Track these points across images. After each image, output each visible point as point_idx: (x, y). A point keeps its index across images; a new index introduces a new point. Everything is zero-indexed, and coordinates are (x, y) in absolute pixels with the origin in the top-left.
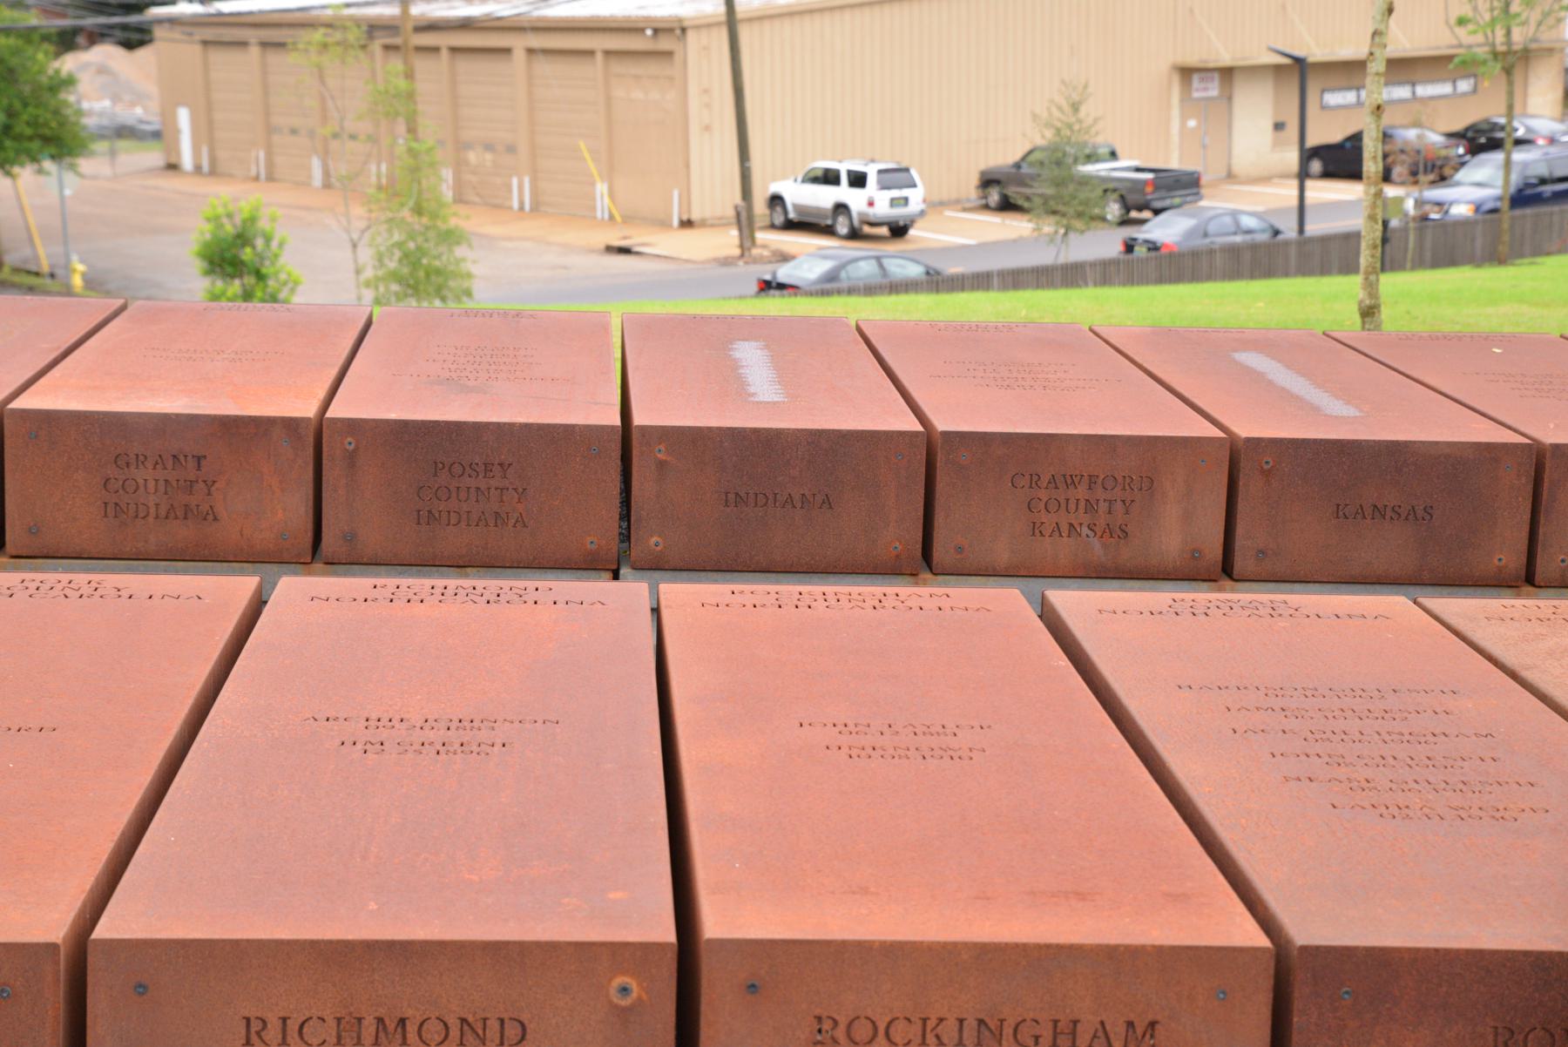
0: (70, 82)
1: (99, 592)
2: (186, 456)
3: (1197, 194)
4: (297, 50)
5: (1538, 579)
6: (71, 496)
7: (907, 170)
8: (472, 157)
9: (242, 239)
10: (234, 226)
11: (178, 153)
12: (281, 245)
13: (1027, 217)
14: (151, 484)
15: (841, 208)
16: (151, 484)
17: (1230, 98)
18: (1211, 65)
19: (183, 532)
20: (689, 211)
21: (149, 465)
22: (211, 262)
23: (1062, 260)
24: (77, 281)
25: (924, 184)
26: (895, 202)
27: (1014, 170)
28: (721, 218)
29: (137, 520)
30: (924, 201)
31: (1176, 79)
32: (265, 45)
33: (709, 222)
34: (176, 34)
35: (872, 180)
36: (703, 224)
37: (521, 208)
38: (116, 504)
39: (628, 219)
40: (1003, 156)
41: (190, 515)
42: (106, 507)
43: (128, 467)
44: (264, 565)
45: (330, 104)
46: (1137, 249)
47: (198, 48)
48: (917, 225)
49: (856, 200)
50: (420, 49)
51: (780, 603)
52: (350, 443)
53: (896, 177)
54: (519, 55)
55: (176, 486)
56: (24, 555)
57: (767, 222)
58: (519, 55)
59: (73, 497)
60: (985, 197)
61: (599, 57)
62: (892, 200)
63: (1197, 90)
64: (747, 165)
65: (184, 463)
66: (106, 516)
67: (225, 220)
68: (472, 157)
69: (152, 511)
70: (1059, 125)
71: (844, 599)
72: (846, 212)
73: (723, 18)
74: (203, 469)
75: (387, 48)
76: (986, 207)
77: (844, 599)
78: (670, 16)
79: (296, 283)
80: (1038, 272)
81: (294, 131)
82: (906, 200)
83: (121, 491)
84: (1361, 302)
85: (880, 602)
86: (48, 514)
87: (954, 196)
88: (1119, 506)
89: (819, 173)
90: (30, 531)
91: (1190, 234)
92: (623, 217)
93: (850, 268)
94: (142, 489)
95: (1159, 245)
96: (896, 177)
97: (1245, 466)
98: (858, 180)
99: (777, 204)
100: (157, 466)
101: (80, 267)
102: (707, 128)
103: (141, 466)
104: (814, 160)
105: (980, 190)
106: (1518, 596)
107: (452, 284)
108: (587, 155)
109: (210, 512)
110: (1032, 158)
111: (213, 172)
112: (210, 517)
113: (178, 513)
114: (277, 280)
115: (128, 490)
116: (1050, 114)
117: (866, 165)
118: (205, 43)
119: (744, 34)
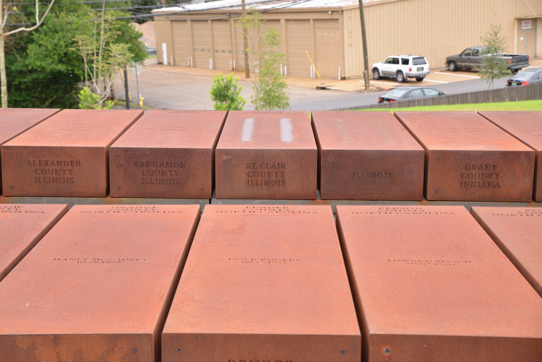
0: (141, 35)
2: (490, 165)
3: (528, 63)
4: (238, 22)
5: (428, 198)
6: (450, 179)
7: (423, 58)
9: (227, 88)
10: (224, 83)
11: (162, 59)
12: (240, 90)
13: (477, 74)
14: (477, 175)
15: (399, 72)
16: (477, 175)
17: (536, 29)
18: (530, 17)
19: (487, 192)
20: (344, 75)
21: (477, 169)
22: (216, 96)
23: (491, 89)
24: (141, 103)
26: (419, 69)
27: (459, 57)
28: (355, 76)
29: (472, 188)
30: (429, 69)
31: (516, 22)
32: (192, 21)
33: (351, 78)
34: (162, 18)
35: (411, 62)
36: (349, 78)
37: (313, 77)
38: (465, 182)
39: (323, 77)
40: (455, 52)
41: (490, 185)
42: (461, 183)
43: (470, 169)
44: (172, 199)
45: (249, 41)
46: (513, 83)
47: (169, 22)
48: (426, 77)
49: (405, 69)
51: (380, 212)
52: (225, 158)
53: (419, 60)
54: (283, 22)
55: (486, 176)
56: (433, 200)
57: (373, 77)
58: (283, 22)
59: (451, 180)
60: (449, 67)
61: (312, 21)
62: (418, 68)
63: (524, 27)
64: (367, 57)
65: (489, 168)
66: (461, 186)
67: (221, 81)
69: (477, 184)
70: (490, 40)
71: (263, 209)
72: (401, 73)
73: (358, 6)
74: (496, 170)
76: (449, 70)
77: (263, 209)
78: (337, 6)
79: (244, 103)
80: (484, 92)
81: (202, 50)
82: (423, 68)
83: (467, 178)
84: (212, 98)
85: (415, 211)
86: (442, 186)
87: (436, 67)
89: (391, 60)
91: (532, 78)
92: (321, 77)
93: (412, 93)
94: (474, 177)
95: (521, 82)
96: (419, 60)
98: (406, 62)
99: (375, 71)
100: (52, 165)
101: (142, 99)
102: (351, 45)
103: (474, 169)
104: (391, 55)
105: (447, 64)
106: (531, 206)
107: (282, 101)
108: (309, 56)
109: (497, 184)
110: (466, 52)
111: (174, 65)
112: (497, 186)
113: (486, 185)
114: (238, 102)
115: (469, 177)
116: (487, 37)
117: (408, 57)
118: (172, 21)
119: (365, 11)
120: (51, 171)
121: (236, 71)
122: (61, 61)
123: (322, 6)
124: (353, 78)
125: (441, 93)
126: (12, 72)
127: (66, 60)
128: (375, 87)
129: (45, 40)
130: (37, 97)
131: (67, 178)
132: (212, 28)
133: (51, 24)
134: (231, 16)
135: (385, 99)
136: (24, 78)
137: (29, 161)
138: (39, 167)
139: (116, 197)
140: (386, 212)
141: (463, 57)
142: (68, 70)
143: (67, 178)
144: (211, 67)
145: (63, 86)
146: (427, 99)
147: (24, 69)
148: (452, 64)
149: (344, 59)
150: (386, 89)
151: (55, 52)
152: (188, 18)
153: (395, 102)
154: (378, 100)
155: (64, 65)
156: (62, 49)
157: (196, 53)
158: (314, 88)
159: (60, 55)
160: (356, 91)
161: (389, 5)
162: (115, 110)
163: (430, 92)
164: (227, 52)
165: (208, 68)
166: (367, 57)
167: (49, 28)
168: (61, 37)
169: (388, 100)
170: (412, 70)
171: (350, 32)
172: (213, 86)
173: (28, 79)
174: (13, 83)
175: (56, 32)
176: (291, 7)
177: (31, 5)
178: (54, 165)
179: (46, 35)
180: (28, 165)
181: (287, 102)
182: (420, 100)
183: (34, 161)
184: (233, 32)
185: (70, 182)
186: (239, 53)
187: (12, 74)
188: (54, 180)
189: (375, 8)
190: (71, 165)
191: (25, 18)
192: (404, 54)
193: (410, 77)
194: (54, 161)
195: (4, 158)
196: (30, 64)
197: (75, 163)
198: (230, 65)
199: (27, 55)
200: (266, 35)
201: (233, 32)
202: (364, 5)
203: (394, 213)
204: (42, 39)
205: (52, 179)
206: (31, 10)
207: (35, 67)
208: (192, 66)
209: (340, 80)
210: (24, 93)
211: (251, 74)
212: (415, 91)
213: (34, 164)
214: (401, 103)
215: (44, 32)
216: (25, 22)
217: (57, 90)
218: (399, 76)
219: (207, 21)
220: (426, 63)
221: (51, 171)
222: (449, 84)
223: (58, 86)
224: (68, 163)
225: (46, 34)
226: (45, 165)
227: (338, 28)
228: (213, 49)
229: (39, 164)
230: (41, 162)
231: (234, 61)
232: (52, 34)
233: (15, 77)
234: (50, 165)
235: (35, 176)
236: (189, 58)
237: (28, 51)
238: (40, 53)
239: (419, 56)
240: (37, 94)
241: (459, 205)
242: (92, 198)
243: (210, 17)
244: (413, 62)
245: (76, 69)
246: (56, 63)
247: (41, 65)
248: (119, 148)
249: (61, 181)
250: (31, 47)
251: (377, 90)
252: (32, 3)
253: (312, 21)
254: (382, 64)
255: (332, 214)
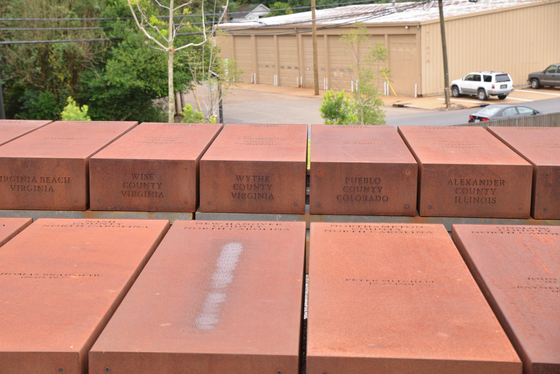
1: (112, 225)
7: (506, 75)
8: (335, 74)
9: (338, 104)
15: (481, 89)
20: (421, 92)
22: (326, 113)
25: (513, 80)
27: (543, 74)
28: (432, 94)
33: (428, 95)
35: (494, 79)
36: (426, 96)
37: (387, 94)
39: (399, 95)
40: (539, 68)
47: (232, 38)
48: (509, 95)
49: (487, 86)
50: (318, 36)
53: (503, 77)
60: (531, 84)
61: (386, 37)
62: (501, 86)
68: (335, 74)
73: (439, 21)
75: (303, 36)
76: (531, 88)
81: (267, 66)
82: (506, 85)
88: (376, 190)
89: (472, 77)
90: (295, 205)
92: (397, 94)
96: (503, 77)
97: (538, 177)
98: (488, 79)
102: (428, 61)
104: (470, 72)
105: (529, 82)
107: (378, 119)
110: (550, 69)
117: (491, 73)
118: (234, 36)
119: (446, 25)
120: (472, 190)
121: (302, 87)
122: (139, 77)
123: (398, 21)
124: (430, 95)
125: (536, 112)
126: (89, 88)
127: (144, 76)
128: (457, 105)
129: (124, 55)
130: (113, 114)
131: (490, 198)
132: (278, 44)
133: (130, 39)
134: (299, 32)
135: (477, 118)
136: (101, 94)
137: (451, 179)
138: (460, 186)
139: (541, 218)
140: (353, 230)
141: (547, 74)
142: (146, 86)
143: (490, 198)
144: (276, 83)
145: (139, 103)
146: (528, 118)
147: (102, 85)
148: (535, 81)
149: (421, 75)
150: (468, 107)
151: (134, 67)
152: (253, 33)
153: (488, 121)
154: (468, 119)
155: (142, 81)
156: (141, 64)
157: (260, 69)
158: (390, 106)
159: (138, 71)
160: (437, 109)
161: (468, 20)
162: (527, 127)
163: (523, 110)
164: (293, 68)
165: (274, 85)
166: (447, 74)
167: (128, 43)
168: (140, 53)
169: (481, 119)
170: (496, 87)
171: (428, 48)
172: (324, 103)
173: (106, 95)
174: (90, 99)
175: (135, 47)
176: (367, 22)
177: (110, 20)
178: (477, 184)
179: (124, 51)
180: (448, 184)
181: (382, 120)
182: (521, 119)
183: (456, 180)
184: (300, 47)
185: (492, 202)
186: (306, 69)
187: (89, 90)
188: (475, 200)
189: (453, 23)
190: (495, 184)
191: (104, 34)
192: (488, 71)
193: (492, 95)
194: (477, 180)
195: (424, 177)
196: (108, 80)
197: (499, 182)
198: (296, 82)
199: (105, 71)
200: (373, 51)
201: (300, 47)
202: (445, 20)
203: (517, 232)
204: (121, 55)
205: (472, 198)
206: (110, 25)
207: (114, 83)
208: (255, 83)
209: (416, 98)
210: (100, 110)
211: (320, 92)
212: (507, 109)
213: (455, 183)
214: (501, 121)
215: (123, 47)
216: (104, 37)
217: (132, 107)
218: (481, 93)
219: (272, 36)
220: (509, 81)
221: (472, 190)
222: (534, 102)
223: (134, 102)
224: (492, 182)
225: (125, 49)
226: (466, 184)
227: (415, 44)
228: (279, 66)
229: (461, 183)
230: (462, 181)
231: (301, 78)
232: (131, 49)
233: (92, 93)
234: (471, 183)
235: (456, 195)
236: (252, 74)
237: (107, 67)
238: (118, 68)
239: (503, 72)
240: (112, 111)
241: (436, 222)
242: (514, 219)
243: (276, 32)
244: (496, 79)
245: (154, 85)
246: (135, 79)
247: (120, 81)
248: (548, 166)
249: (483, 201)
250: (109, 62)
251: (459, 108)
252: (111, 18)
253: (325, 37)
254: (462, 81)
255: (447, 233)
